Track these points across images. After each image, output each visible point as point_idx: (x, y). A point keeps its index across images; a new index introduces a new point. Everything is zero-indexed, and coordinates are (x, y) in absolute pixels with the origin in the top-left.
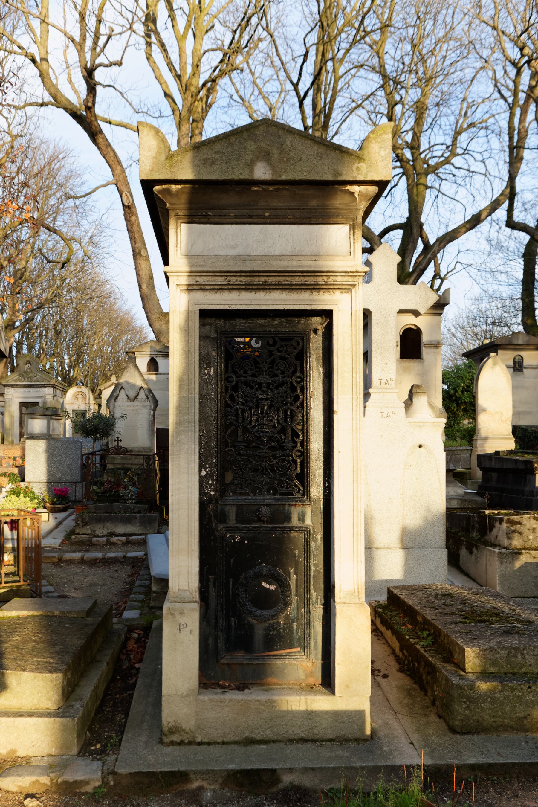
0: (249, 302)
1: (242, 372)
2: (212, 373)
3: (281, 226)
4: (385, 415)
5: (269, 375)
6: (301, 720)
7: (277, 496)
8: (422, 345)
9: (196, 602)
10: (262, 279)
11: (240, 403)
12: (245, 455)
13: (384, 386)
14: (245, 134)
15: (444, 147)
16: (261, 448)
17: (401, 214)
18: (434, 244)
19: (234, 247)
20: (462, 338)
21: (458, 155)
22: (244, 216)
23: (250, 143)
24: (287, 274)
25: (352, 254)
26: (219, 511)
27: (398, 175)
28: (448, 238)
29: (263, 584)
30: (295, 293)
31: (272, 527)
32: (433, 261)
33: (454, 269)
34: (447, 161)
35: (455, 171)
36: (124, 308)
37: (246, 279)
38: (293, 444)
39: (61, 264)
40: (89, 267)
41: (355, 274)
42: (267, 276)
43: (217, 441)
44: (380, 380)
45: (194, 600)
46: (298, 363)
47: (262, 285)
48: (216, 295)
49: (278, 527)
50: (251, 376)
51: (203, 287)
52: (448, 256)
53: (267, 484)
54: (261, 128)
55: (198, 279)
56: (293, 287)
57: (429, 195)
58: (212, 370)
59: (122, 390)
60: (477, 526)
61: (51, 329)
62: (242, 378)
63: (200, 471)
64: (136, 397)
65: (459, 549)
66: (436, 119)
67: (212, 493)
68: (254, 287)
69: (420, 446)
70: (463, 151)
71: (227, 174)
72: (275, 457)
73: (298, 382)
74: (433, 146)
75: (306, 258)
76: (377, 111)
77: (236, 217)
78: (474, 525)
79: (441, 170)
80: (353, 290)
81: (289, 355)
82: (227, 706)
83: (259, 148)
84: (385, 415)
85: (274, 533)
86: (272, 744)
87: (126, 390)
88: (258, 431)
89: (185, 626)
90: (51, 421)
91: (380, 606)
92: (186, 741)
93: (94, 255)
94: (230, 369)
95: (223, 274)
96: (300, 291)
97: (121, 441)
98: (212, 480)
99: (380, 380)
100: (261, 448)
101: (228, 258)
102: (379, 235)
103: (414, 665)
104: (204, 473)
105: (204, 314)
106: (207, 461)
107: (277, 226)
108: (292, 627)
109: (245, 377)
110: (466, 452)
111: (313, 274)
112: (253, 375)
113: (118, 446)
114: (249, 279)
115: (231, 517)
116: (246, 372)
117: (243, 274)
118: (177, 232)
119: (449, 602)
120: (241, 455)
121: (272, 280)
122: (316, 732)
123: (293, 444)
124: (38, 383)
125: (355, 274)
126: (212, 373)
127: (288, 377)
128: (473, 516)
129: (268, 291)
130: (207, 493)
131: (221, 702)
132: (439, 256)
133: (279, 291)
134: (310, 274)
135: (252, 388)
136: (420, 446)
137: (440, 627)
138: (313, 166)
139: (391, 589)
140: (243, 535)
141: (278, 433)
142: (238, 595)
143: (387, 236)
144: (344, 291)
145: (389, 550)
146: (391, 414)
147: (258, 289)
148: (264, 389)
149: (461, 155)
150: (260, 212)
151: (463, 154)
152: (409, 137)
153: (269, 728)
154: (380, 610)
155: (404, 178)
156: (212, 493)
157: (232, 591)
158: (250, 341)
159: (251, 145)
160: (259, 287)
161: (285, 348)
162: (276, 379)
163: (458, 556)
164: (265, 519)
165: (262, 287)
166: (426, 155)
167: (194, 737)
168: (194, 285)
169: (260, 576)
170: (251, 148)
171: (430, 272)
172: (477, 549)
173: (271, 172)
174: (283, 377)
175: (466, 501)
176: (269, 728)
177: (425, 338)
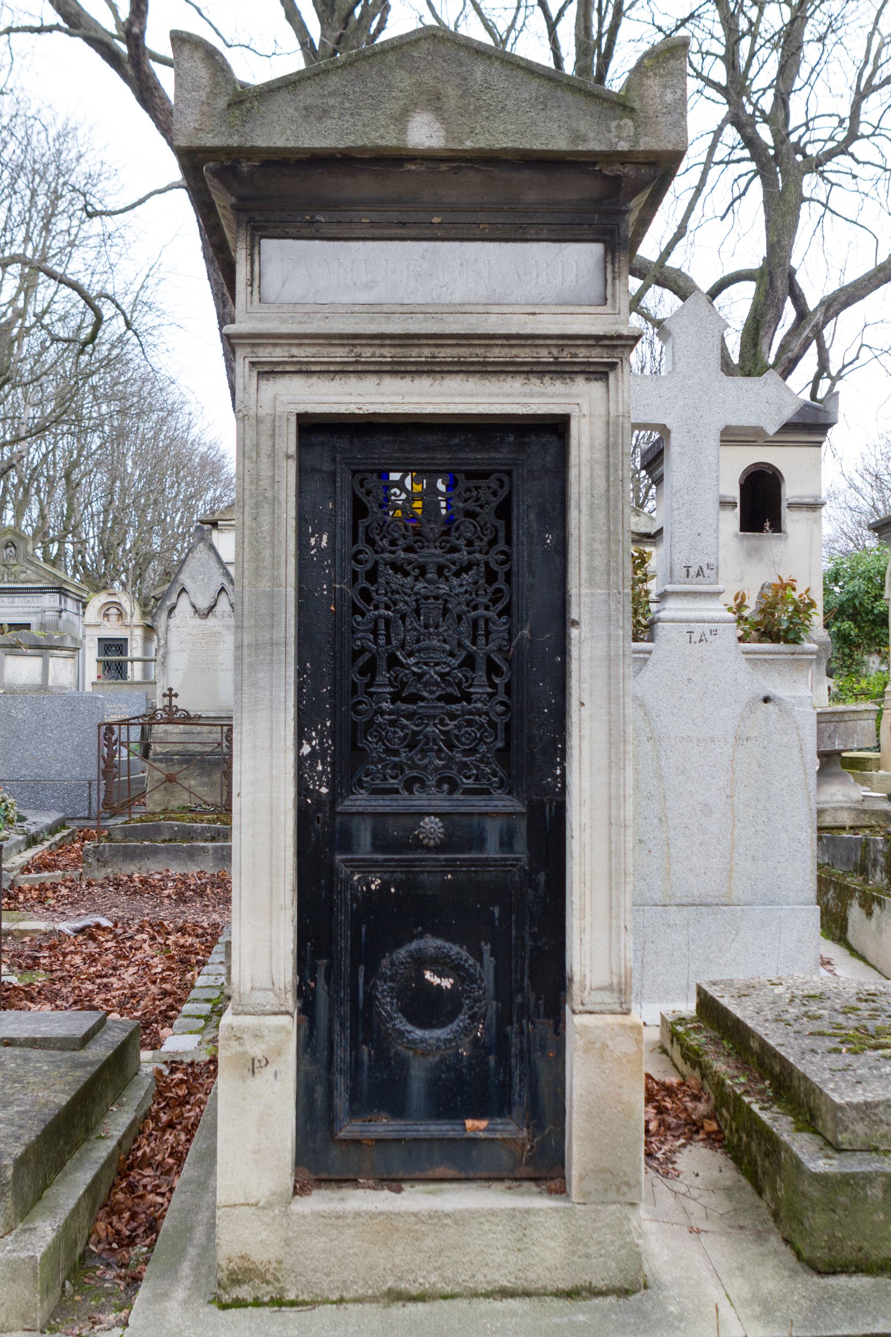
0: (399, 399)
1: (385, 543)
2: (324, 544)
3: (465, 244)
4: (696, 637)
5: (442, 548)
6: (501, 1252)
7: (457, 795)
8: (784, 504)
9: (287, 1013)
10: (427, 352)
11: (382, 605)
12: (391, 713)
13: (695, 580)
14: (391, 58)
15: (835, 120)
16: (423, 699)
17: (753, 253)
18: (816, 310)
19: (368, 286)
20: (876, 495)
21: (863, 136)
22: (389, 224)
23: (400, 74)
24: (476, 342)
25: (609, 302)
26: (337, 826)
27: (746, 174)
28: (843, 299)
29: (428, 975)
30: (494, 380)
31: (446, 860)
32: (814, 343)
33: (857, 358)
34: (842, 149)
35: (857, 169)
36: (207, 438)
37: (393, 351)
38: (490, 690)
39: (78, 346)
40: (132, 351)
41: (615, 342)
42: (436, 346)
43: (334, 684)
44: (688, 568)
45: (283, 1009)
46: (500, 524)
47: (426, 363)
48: (333, 383)
49: (458, 859)
50: (405, 550)
51: (304, 368)
52: (843, 333)
53: (437, 769)
54: (425, 45)
55: (295, 351)
56: (490, 369)
57: (808, 214)
58: (325, 537)
59: (184, 595)
60: (882, 860)
61: (60, 478)
62: (386, 555)
63: (299, 746)
64: (211, 608)
65: (845, 907)
66: (818, 69)
67: (324, 790)
68: (409, 368)
69: (766, 700)
70: (871, 130)
71: (352, 137)
72: (452, 716)
73: (503, 563)
74: (813, 119)
75: (517, 309)
76: (704, 50)
77: (373, 224)
78: (875, 860)
79: (829, 166)
80: (611, 376)
81: (482, 507)
82: (349, 1226)
83: (418, 84)
84: (696, 637)
85: (451, 872)
86: (442, 1301)
87: (191, 594)
88: (417, 663)
89: (264, 1062)
90: (52, 661)
91: (682, 1020)
92: (266, 1299)
93: (143, 328)
94: (361, 535)
95: (345, 342)
96: (503, 377)
97: (176, 695)
98: (323, 764)
99: (688, 568)
100: (423, 699)
101: (356, 309)
102: (708, 293)
103: (740, 1139)
104: (306, 749)
105: (313, 428)
106: (312, 725)
107: (457, 244)
108: (487, 1064)
109: (393, 552)
110: (865, 716)
111: (530, 342)
112: (409, 549)
113: (170, 706)
114: (398, 351)
115: (362, 840)
116: (393, 543)
117: (388, 342)
118: (252, 255)
119: (814, 1008)
120: (382, 713)
121: (445, 354)
122: (531, 1276)
123: (490, 690)
124: (30, 585)
125: (615, 342)
126: (324, 544)
127: (480, 552)
128: (875, 841)
129: (438, 376)
130: (313, 790)
131: (338, 1217)
132: (827, 332)
133: (461, 376)
134: (523, 342)
135: (406, 574)
136: (766, 700)
137: (791, 1060)
138: (528, 122)
139: (705, 987)
140: (386, 877)
141: (461, 666)
142: (376, 998)
143: (725, 293)
144: (592, 376)
145: (704, 909)
146: (708, 636)
147: (416, 372)
148: (430, 576)
149: (868, 137)
150: (422, 217)
151: (873, 134)
152: (767, 103)
153: (436, 1269)
154: (680, 1029)
155: (758, 180)
156: (324, 790)
157: (365, 993)
158: (403, 478)
159: (403, 80)
160: (420, 368)
161: (474, 493)
162: (456, 556)
163: (845, 919)
164: (432, 843)
165: (426, 368)
166: (800, 138)
167: (282, 1290)
168: (285, 363)
169: (420, 961)
170: (402, 85)
171: (808, 364)
172: (880, 904)
173: (443, 133)
174: (469, 553)
175: (864, 812)
176: (436, 1269)
177: (790, 491)
